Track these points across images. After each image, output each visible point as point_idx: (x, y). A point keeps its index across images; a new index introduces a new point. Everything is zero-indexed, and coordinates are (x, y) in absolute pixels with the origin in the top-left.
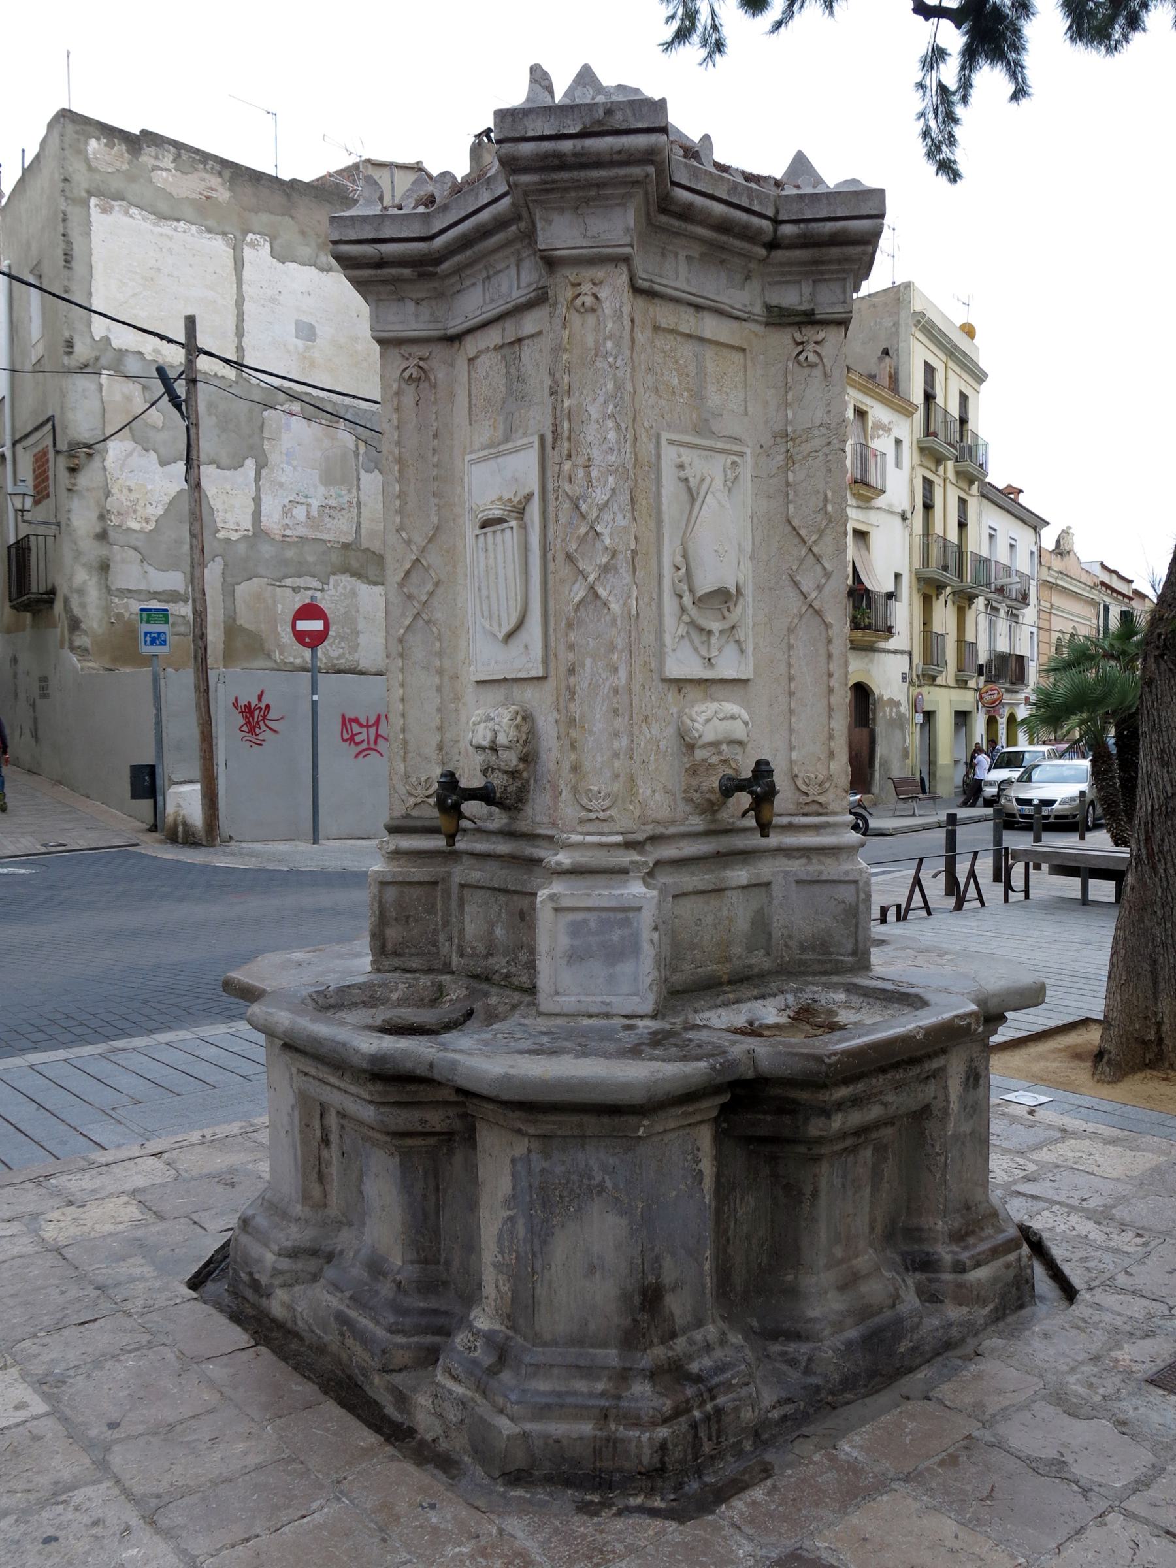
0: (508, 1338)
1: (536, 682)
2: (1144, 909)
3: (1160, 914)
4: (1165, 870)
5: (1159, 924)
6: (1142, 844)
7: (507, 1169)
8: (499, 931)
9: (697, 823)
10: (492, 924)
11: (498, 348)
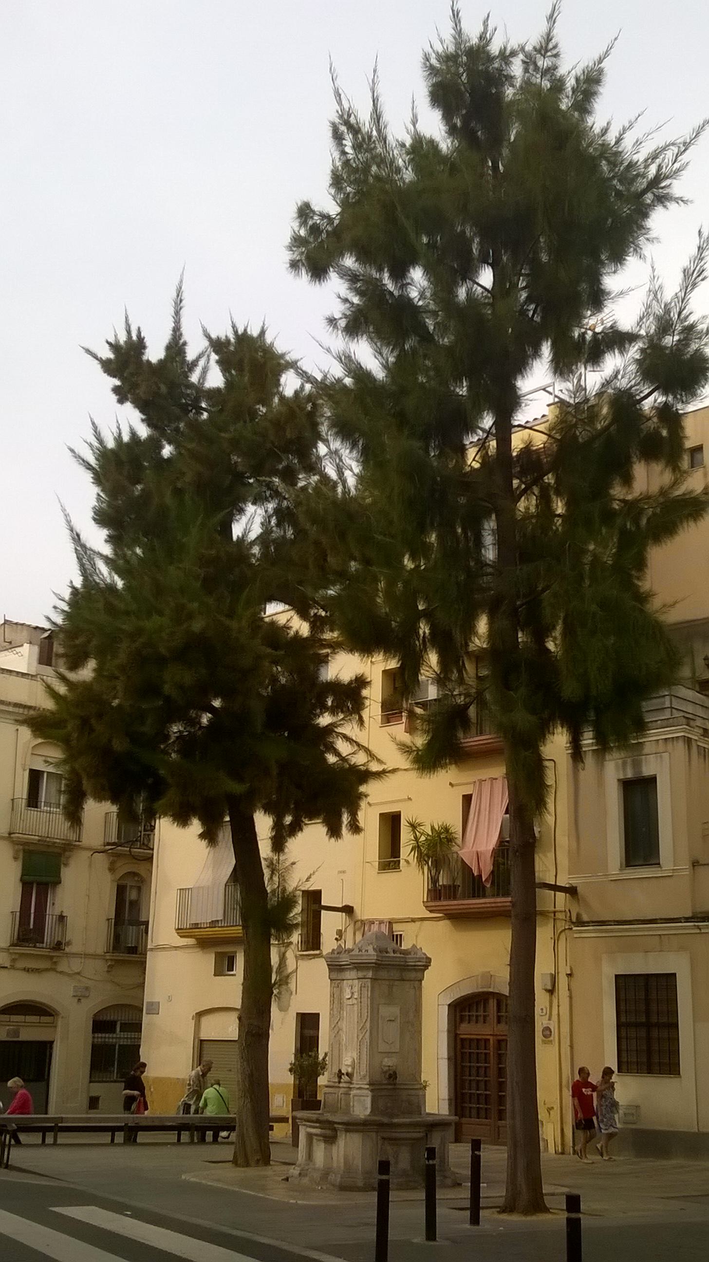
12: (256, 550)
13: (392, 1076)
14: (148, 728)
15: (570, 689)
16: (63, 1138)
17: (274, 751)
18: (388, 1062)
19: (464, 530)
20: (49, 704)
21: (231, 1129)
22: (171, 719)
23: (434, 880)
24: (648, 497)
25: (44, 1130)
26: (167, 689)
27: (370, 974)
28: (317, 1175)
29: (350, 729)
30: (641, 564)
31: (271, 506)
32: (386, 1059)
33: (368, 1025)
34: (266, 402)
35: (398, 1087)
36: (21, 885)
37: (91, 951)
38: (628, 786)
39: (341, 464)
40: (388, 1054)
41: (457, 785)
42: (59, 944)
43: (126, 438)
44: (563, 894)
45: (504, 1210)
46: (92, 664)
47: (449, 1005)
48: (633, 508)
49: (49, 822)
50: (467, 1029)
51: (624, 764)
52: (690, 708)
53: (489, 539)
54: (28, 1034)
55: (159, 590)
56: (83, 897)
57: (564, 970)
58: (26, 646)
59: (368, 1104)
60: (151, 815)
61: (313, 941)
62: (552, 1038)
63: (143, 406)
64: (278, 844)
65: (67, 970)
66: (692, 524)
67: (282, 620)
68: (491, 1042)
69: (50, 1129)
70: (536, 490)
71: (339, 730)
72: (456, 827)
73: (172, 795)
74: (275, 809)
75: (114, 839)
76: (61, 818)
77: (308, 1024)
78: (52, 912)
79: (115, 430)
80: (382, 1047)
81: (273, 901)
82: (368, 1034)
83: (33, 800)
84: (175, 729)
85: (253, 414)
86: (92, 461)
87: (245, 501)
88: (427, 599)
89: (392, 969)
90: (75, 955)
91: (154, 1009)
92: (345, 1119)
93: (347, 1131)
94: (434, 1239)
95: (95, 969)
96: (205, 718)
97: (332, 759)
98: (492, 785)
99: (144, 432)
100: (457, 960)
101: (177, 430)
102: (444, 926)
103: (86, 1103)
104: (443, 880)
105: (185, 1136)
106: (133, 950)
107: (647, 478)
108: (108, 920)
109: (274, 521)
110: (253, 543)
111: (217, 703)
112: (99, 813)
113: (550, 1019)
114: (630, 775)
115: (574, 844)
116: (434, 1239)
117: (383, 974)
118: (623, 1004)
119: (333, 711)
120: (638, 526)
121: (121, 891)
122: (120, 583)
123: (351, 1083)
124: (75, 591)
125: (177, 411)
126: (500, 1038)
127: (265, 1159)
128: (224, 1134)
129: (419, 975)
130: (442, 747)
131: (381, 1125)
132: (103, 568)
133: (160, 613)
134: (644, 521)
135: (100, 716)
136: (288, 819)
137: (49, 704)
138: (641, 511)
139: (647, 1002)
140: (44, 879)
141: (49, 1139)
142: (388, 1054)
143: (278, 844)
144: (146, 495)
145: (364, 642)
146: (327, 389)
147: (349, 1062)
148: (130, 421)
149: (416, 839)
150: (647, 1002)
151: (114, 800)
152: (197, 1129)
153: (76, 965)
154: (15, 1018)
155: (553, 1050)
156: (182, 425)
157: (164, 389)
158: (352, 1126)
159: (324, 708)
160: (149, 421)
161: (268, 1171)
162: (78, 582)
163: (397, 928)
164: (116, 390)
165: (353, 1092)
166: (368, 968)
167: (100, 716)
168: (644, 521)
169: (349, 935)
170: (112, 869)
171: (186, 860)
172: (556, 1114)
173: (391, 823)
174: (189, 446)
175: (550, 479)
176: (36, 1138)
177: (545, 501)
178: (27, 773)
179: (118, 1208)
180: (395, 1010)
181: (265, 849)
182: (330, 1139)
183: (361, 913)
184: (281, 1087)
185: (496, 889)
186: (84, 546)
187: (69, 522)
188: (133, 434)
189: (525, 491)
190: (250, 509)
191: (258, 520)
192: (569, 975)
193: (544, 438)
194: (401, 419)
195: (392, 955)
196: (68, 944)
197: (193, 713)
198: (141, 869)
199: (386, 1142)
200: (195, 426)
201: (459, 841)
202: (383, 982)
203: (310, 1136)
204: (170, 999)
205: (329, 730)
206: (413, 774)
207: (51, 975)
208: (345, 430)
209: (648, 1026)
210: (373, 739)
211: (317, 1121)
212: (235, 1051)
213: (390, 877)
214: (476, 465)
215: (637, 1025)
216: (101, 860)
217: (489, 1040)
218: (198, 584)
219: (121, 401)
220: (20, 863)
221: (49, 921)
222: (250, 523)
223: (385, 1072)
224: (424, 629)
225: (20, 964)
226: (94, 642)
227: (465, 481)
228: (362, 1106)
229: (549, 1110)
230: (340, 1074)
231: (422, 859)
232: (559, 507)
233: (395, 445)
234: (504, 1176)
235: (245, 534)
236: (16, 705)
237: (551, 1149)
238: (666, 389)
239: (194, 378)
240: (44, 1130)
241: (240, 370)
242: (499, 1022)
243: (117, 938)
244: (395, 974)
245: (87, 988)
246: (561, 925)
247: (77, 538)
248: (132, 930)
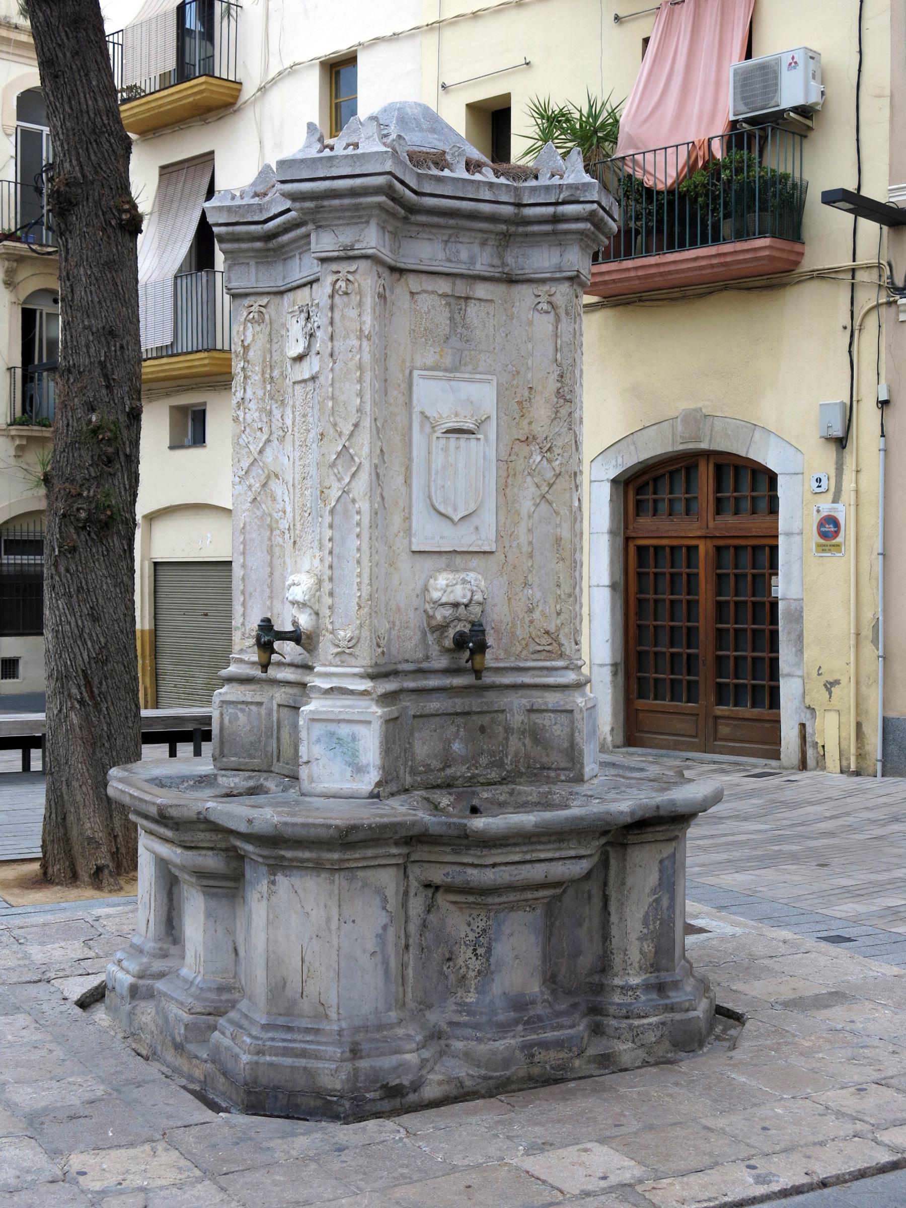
0: (657, 977)
1: (436, 556)
2: (95, 743)
3: (107, 745)
4: (107, 708)
5: (106, 753)
6: (83, 688)
7: (656, 867)
8: (456, 746)
9: (442, 662)
10: (449, 742)
11: (445, 295)
13: (469, 642)
18: (448, 586)
32: (442, 580)
33: (363, 447)
35: (488, 679)
40: (452, 557)
41: (634, 16)
44: (875, 226)
47: (614, 481)
50: (659, 528)
57: (870, 392)
59: (370, 745)
62: (839, 540)
68: (702, 550)
80: (428, 533)
82: (364, 477)
93: (277, 866)
108: (9, 369)
113: (836, 500)
117: (426, 251)
123: (308, 668)
126: (721, 543)
131: (414, 839)
142: (452, 557)
165: (312, 706)
172: (845, 694)
180: (481, 396)
192: (884, 404)
195: (463, 174)
199: (442, 899)
202: (429, 284)
217: (697, 547)
223: (441, 628)
228: (342, 758)
229: (830, 686)
242: (718, 511)
243: (28, 399)
246: (867, 298)
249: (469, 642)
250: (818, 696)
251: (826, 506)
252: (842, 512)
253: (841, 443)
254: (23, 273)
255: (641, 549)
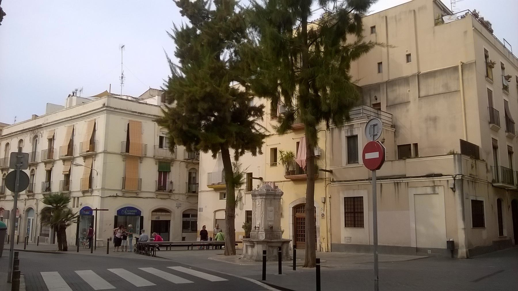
12: (227, 64)
14: (194, 123)
15: (324, 108)
16: (172, 248)
17: (234, 129)
18: (270, 223)
19: (291, 57)
20: (163, 115)
21: (224, 245)
22: (202, 119)
23: (288, 169)
24: (350, 45)
25: (167, 246)
26: (199, 110)
27: (264, 197)
28: (249, 257)
29: (259, 121)
30: (348, 67)
31: (232, 50)
34: (230, 15)
36: (158, 173)
37: (181, 192)
38: (349, 138)
39: (254, 36)
42: (171, 190)
43: (185, 28)
45: (304, 266)
46: (176, 102)
48: (346, 49)
49: (165, 153)
50: (298, 215)
51: (348, 131)
52: (369, 113)
53: (299, 60)
54: (162, 218)
55: (196, 78)
56: (178, 176)
57: (328, 196)
58: (157, 96)
60: (197, 150)
61: (250, 188)
63: (190, 17)
64: (237, 158)
65: (173, 198)
66: (365, 54)
67: (236, 87)
69: (169, 246)
70: (315, 43)
71: (256, 122)
72: (295, 152)
73: (202, 143)
74: (236, 147)
75: (187, 158)
76: (168, 151)
77: (249, 214)
78: (168, 181)
79: (181, 25)
80: (268, 219)
81: (235, 176)
83: (161, 146)
84: (203, 122)
85: (226, 19)
86: (174, 36)
87: (224, 48)
88: (281, 80)
89: (272, 195)
90: (176, 194)
91: (201, 210)
92: (257, 240)
94: (281, 274)
95: (182, 198)
96: (212, 119)
97: (253, 131)
98: (302, 137)
99: (191, 26)
100: (292, 194)
101: (201, 24)
102: (291, 183)
103: (181, 239)
104: (291, 169)
105: (211, 247)
106: (194, 192)
107: (351, 39)
109: (233, 55)
110: (226, 62)
111: (216, 114)
112: (181, 149)
114: (349, 135)
115: (332, 157)
116: (281, 274)
117: (268, 197)
118: (346, 206)
119: (254, 116)
120: (347, 55)
121: (190, 174)
122: (184, 76)
124: (170, 79)
125: (201, 18)
127: (234, 253)
128: (223, 247)
129: (280, 197)
130: (286, 126)
131: (268, 242)
132: (178, 71)
133: (197, 86)
134: (349, 53)
135: (178, 119)
136: (240, 150)
137: (163, 115)
138: (349, 50)
139: (354, 205)
140: (165, 170)
141: (169, 249)
143: (237, 158)
144: (191, 48)
145: (263, 93)
146: (248, 11)
147: (258, 223)
148: (186, 22)
149: (282, 156)
150: (354, 205)
151: (185, 145)
152: (218, 246)
153: (176, 197)
154: (158, 213)
155: (324, 221)
156: (203, 23)
157: (196, 11)
158: (259, 242)
159: (251, 115)
160: (192, 22)
161: (235, 256)
162: (171, 76)
163: (276, 184)
164: (181, 12)
166: (263, 196)
167: (178, 119)
168: (349, 53)
169: (261, 186)
170: (187, 167)
171: (210, 164)
172: (326, 240)
173: (274, 151)
174: (205, 30)
175: (319, 40)
176: (165, 249)
177: (317, 47)
178: (158, 137)
179: (188, 267)
181: (232, 160)
182: (253, 247)
183: (265, 180)
184: (240, 233)
185: (307, 172)
186: (172, 64)
187: (167, 56)
188: (187, 26)
189: (311, 44)
190: (226, 50)
191: (228, 55)
193: (317, 26)
194: (270, 22)
196: (174, 190)
197: (208, 117)
198: (196, 167)
200: (207, 23)
201: (295, 157)
203: (247, 246)
204: (206, 207)
205: (253, 122)
206: (277, 135)
207: (169, 200)
208: (254, 26)
209: (354, 213)
210: (266, 124)
211: (249, 241)
212: (225, 221)
213: (274, 168)
214: (296, 36)
215: (351, 213)
216: (183, 165)
218: (209, 76)
219: (183, 16)
220: (158, 165)
221: (168, 183)
222: (226, 55)
224: (280, 89)
225: (159, 197)
226: (176, 95)
227: (292, 41)
229: (324, 239)
230: (255, 227)
231: (284, 162)
232: (322, 49)
233: (270, 30)
234: (304, 257)
235: (224, 60)
236: (154, 116)
237: (324, 251)
238: (356, 8)
239: (206, 7)
240: (167, 246)
241: (222, 4)
243: (189, 188)
244: (273, 197)
245: (180, 204)
246: (327, 182)
247: (170, 61)
248: (194, 186)
249: (272, 228)
250: (322, 240)
251: (322, 212)
252: (325, 213)
253: (324, 203)
254: (189, 165)
255: (297, 218)
